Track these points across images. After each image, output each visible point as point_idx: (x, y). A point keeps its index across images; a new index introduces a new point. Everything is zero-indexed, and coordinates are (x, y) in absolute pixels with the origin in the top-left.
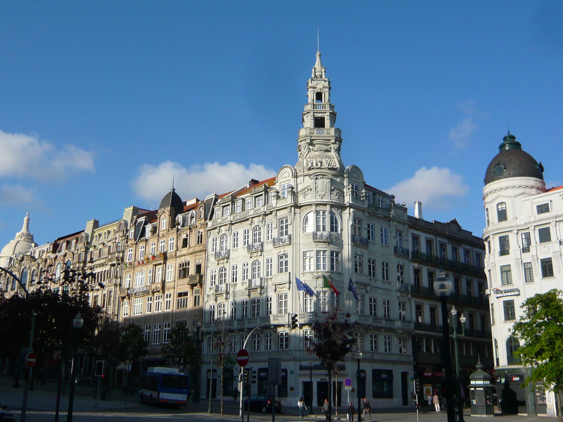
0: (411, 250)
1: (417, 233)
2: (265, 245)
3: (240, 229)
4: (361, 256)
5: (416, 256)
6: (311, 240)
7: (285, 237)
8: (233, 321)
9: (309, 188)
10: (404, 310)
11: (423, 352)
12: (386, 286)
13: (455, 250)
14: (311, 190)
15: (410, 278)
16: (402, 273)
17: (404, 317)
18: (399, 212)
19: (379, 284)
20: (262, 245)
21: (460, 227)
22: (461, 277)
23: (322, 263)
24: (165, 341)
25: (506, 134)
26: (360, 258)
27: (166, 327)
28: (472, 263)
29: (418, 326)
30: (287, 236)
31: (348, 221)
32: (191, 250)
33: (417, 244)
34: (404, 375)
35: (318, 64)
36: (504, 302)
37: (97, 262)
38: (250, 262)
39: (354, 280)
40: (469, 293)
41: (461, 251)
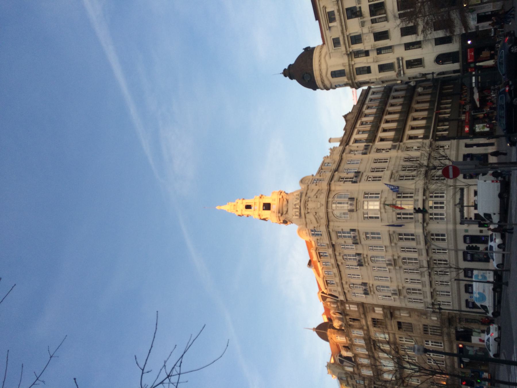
0: (365, 144)
1: (352, 140)
5: (372, 139)
8: (422, 282)
9: (315, 214)
10: (412, 148)
11: (448, 134)
13: (366, 116)
15: (388, 144)
16: (383, 150)
17: (418, 147)
18: (335, 152)
21: (350, 113)
22: (387, 110)
24: (441, 346)
25: (283, 75)
26: (370, 178)
27: (429, 344)
28: (377, 104)
29: (425, 137)
31: (340, 185)
33: (360, 140)
34: (467, 146)
35: (224, 208)
36: (407, 68)
40: (401, 105)
41: (367, 111)
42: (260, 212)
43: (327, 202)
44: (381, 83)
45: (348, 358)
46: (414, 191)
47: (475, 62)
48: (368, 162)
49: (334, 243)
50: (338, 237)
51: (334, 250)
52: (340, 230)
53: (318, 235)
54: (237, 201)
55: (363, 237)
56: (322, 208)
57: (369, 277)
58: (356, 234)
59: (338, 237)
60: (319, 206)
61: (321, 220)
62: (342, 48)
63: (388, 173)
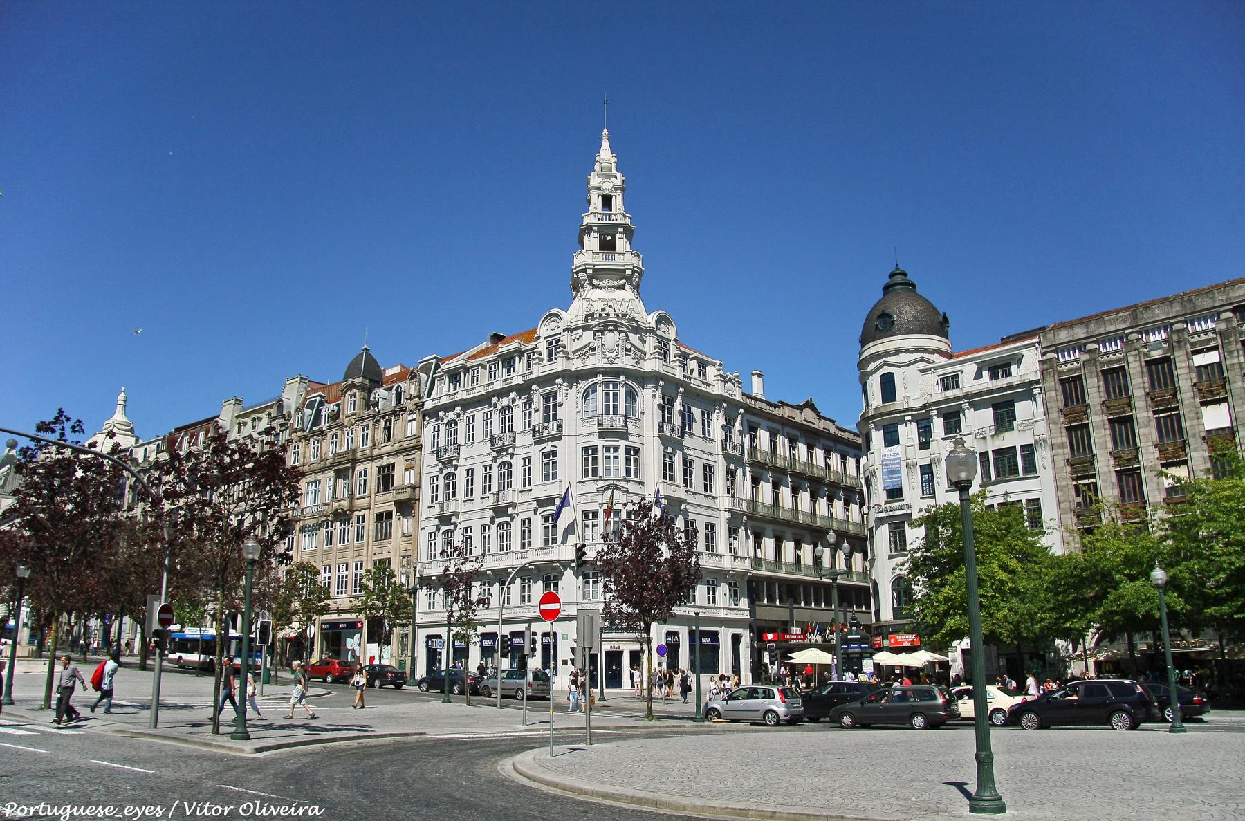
2: (518, 437)
3: (479, 414)
6: (595, 429)
12: (709, 503)
14: (594, 349)
19: (700, 500)
30: (555, 423)
32: (396, 447)
34: (736, 639)
35: (605, 145)
37: (384, 450)
39: (662, 493)
43: (617, 372)
44: (868, 474)
45: (317, 419)
47: (171, 570)
48: (705, 453)
53: (550, 354)
54: (619, 175)
55: (548, 447)
57: (472, 458)
60: (608, 355)
62: (939, 395)
63: (680, 493)
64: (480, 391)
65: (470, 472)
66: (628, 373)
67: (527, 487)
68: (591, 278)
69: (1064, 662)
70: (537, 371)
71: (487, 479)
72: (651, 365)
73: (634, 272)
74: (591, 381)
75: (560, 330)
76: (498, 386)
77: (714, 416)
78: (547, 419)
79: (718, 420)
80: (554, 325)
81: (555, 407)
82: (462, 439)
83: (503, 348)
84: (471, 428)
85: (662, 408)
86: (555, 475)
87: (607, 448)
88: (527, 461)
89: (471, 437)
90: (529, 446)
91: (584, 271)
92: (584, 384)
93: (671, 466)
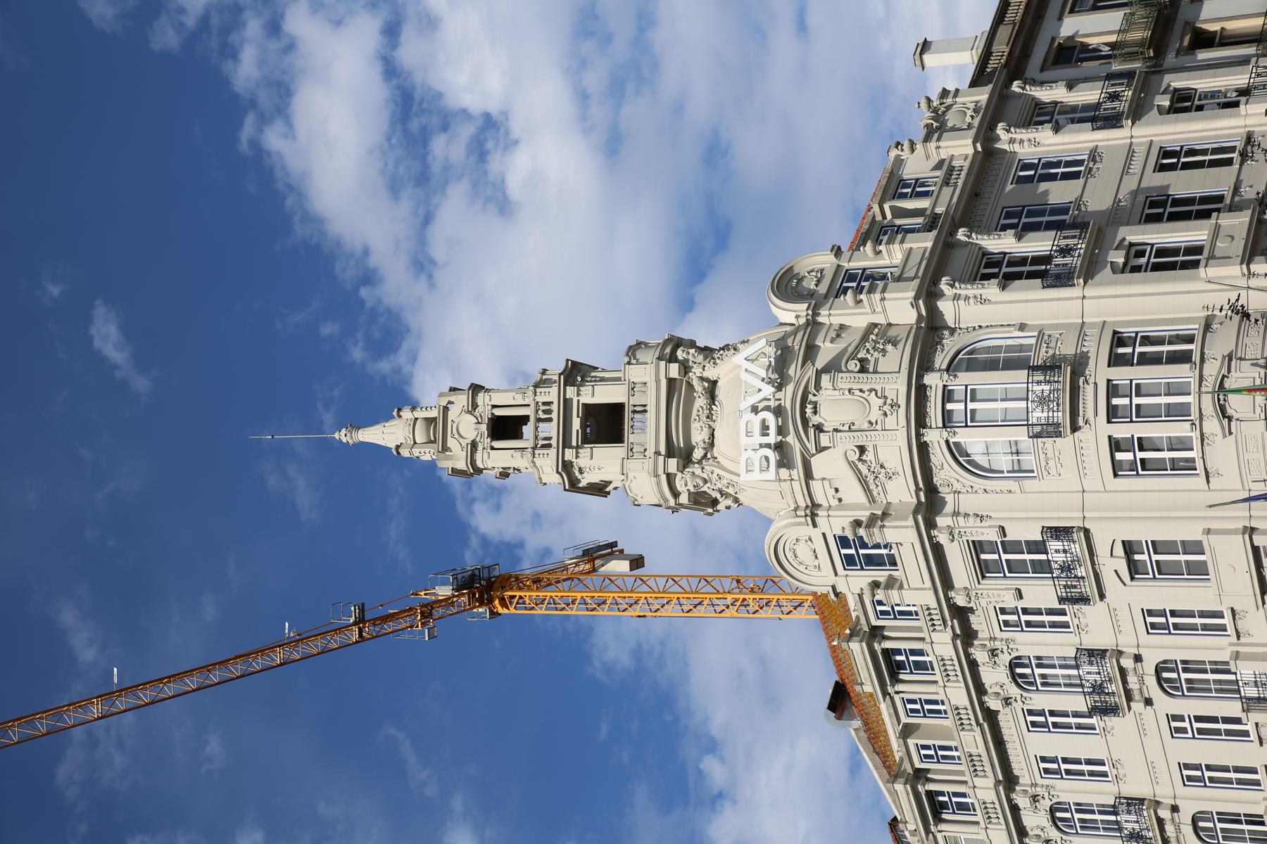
2: (1091, 641)
3: (1027, 747)
4: (1136, 251)
6: (1064, 444)
7: (1056, 552)
9: (854, 457)
14: (862, 449)
20: (1092, 653)
23: (1166, 348)
31: (983, 301)
38: (1166, 705)
42: (569, 454)
46: (1195, 328)
49: (961, 601)
50: (984, 569)
51: (967, 636)
52: (992, 536)
53: (872, 561)
56: (890, 422)
57: (1150, 766)
58: (1078, 548)
59: (984, 569)
60: (875, 415)
61: (889, 485)
64: (974, 741)
65: (1193, 774)
66: (923, 363)
67: (1227, 621)
68: (686, 458)
69: (941, 295)
70: (917, 591)
71: (1207, 727)
72: (900, 309)
73: (673, 359)
74: (939, 456)
75: (816, 534)
76: (958, 695)
77: (1026, 152)
78: (1042, 568)
79: (1040, 143)
80: (804, 552)
81: (1009, 547)
82: (1099, 793)
83: (866, 682)
84: (1068, 767)
85: (1010, 278)
86: (1194, 547)
87: (1113, 414)
88: (1159, 621)
89: (1095, 769)
90: (1112, 612)
91: (670, 478)
92: (946, 472)
93: (1161, 252)
